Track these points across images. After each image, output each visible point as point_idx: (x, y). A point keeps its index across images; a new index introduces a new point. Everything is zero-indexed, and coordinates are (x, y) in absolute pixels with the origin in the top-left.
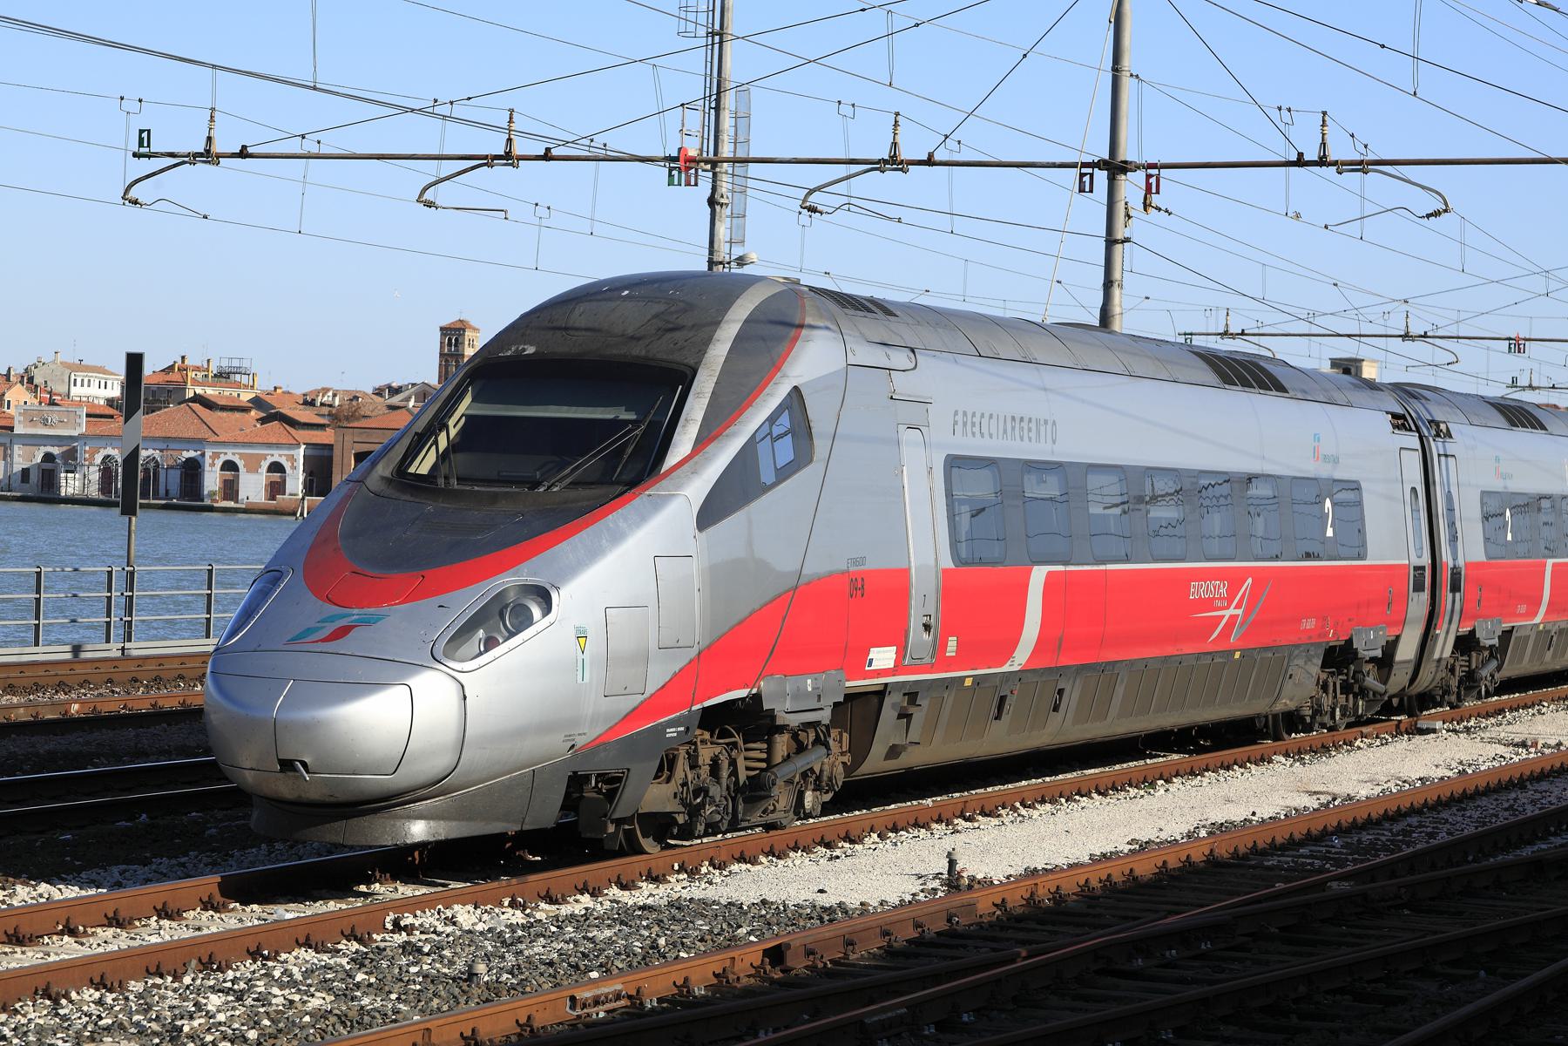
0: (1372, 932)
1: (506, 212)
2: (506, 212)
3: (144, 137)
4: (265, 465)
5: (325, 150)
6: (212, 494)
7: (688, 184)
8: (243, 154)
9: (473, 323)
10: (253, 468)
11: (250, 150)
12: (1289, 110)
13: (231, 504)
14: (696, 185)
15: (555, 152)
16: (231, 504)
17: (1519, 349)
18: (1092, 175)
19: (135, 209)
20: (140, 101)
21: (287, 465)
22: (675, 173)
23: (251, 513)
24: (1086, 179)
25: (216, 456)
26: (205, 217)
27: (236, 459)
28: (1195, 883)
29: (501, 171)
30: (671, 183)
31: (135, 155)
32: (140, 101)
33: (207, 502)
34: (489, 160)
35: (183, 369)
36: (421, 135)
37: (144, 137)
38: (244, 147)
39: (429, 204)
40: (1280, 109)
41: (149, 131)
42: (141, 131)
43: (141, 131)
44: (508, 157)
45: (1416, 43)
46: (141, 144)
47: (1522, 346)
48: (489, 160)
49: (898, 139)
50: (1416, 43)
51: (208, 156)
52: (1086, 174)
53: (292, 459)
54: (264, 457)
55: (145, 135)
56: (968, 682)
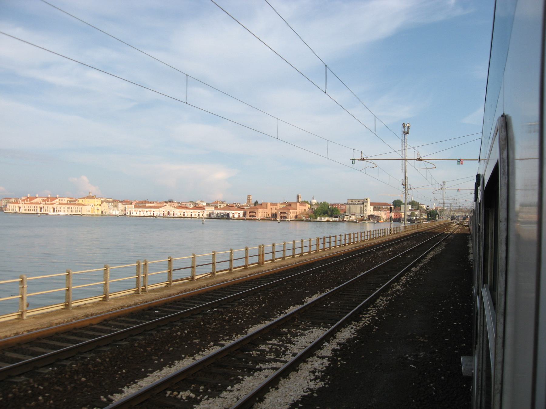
0: (88, 265)
4: (238, 213)
6: (231, 217)
7: (461, 164)
9: (251, 195)
10: (236, 214)
12: (355, 150)
14: (463, 164)
17: (461, 163)
18: (354, 161)
21: (240, 213)
22: (459, 162)
23: (484, 270)
24: (353, 162)
25: (232, 212)
27: (174, 211)
30: (458, 164)
33: (231, 218)
35: (217, 201)
40: (353, 149)
47: (462, 162)
53: (232, 212)
56: (473, 371)
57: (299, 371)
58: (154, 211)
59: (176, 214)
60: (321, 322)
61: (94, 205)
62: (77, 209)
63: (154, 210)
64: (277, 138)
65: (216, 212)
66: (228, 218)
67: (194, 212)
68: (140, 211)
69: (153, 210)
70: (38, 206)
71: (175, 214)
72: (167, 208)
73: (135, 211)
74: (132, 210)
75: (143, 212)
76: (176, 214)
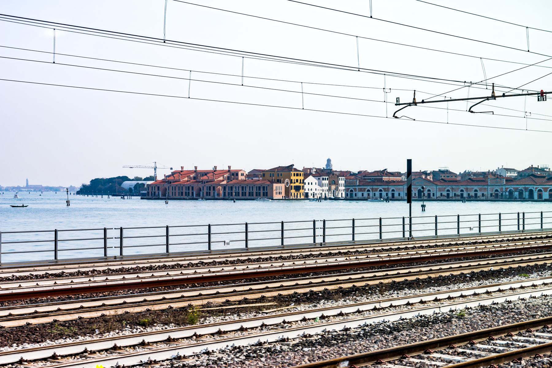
1: (493, 112)
2: (493, 112)
3: (398, 99)
5: (446, 99)
7: (543, 100)
8: (423, 102)
11: (425, 101)
13: (541, 200)
14: (546, 100)
15: (506, 94)
16: (541, 200)
18: (546, 96)
19: (397, 119)
20: (390, 89)
25: (536, 188)
26: (414, 120)
27: (430, 189)
28: (100, 297)
29: (491, 101)
30: (539, 100)
31: (396, 105)
32: (390, 89)
34: (488, 98)
36: (464, 93)
37: (398, 99)
38: (423, 100)
39: (472, 112)
41: (399, 98)
42: (397, 98)
43: (397, 98)
44: (494, 97)
45: (482, 64)
46: (397, 102)
48: (488, 98)
49: (415, 97)
50: (482, 64)
51: (415, 103)
52: (539, 96)
54: (378, 188)
55: (398, 99)
57: (542, 364)
58: (393, 190)
59: (433, 194)
60: (311, 273)
61: (289, 183)
62: (251, 189)
63: (394, 189)
64: (189, 98)
65: (508, 188)
66: (448, 199)
67: (467, 189)
68: (369, 191)
69: (392, 188)
70: (504, 187)
71: (432, 195)
72: (417, 184)
73: (361, 190)
74: (355, 189)
75: (374, 192)
76: (433, 194)
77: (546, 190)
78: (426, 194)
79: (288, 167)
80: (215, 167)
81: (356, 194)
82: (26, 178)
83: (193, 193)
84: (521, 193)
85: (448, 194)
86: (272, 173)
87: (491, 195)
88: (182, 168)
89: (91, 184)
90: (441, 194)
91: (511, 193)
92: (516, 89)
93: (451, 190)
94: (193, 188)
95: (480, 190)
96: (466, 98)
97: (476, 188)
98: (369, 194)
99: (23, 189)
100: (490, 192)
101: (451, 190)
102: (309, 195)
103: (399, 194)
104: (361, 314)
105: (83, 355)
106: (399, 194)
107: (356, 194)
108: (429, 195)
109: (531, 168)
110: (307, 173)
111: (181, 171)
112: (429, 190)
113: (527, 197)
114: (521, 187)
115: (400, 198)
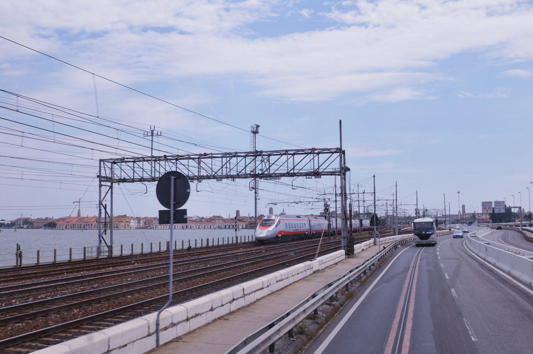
59: (193, 227)
67: (207, 225)
71: (192, 227)
76: (193, 227)
77: (240, 225)
78: (190, 227)
79: (124, 215)
80: (95, 215)
81: (158, 227)
82: (248, 213)
83: (63, 228)
84: (229, 226)
85: (211, 227)
86: (117, 218)
87: (217, 227)
88: (88, 216)
89: (6, 224)
90: (208, 227)
91: (225, 226)
92: (130, 167)
93: (200, 225)
94: (81, 225)
95: (213, 225)
96: (106, 173)
97: (210, 224)
98: (164, 227)
99: (348, 212)
100: (216, 226)
101: (200, 225)
102: (132, 227)
103: (178, 227)
104: (499, 228)
105: (110, 269)
106: (178, 227)
107: (158, 227)
108: (191, 227)
109: (214, 216)
110: (132, 218)
111: (87, 217)
112: (191, 225)
113: (232, 228)
114: (229, 224)
115: (178, 228)
